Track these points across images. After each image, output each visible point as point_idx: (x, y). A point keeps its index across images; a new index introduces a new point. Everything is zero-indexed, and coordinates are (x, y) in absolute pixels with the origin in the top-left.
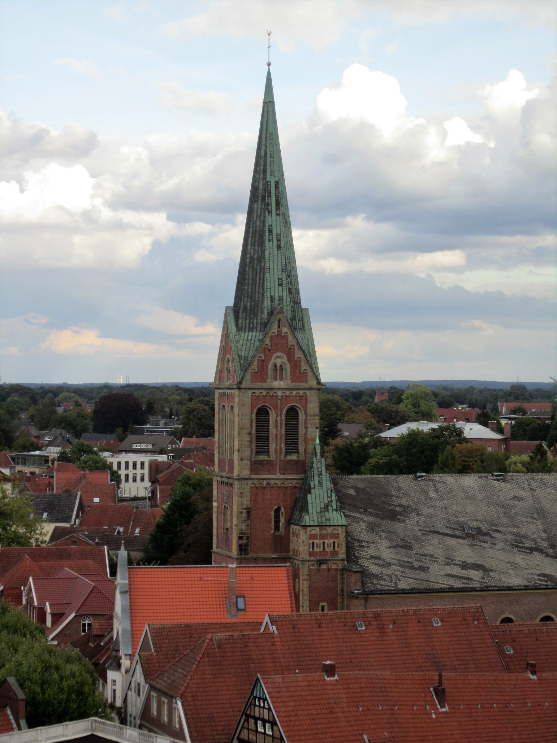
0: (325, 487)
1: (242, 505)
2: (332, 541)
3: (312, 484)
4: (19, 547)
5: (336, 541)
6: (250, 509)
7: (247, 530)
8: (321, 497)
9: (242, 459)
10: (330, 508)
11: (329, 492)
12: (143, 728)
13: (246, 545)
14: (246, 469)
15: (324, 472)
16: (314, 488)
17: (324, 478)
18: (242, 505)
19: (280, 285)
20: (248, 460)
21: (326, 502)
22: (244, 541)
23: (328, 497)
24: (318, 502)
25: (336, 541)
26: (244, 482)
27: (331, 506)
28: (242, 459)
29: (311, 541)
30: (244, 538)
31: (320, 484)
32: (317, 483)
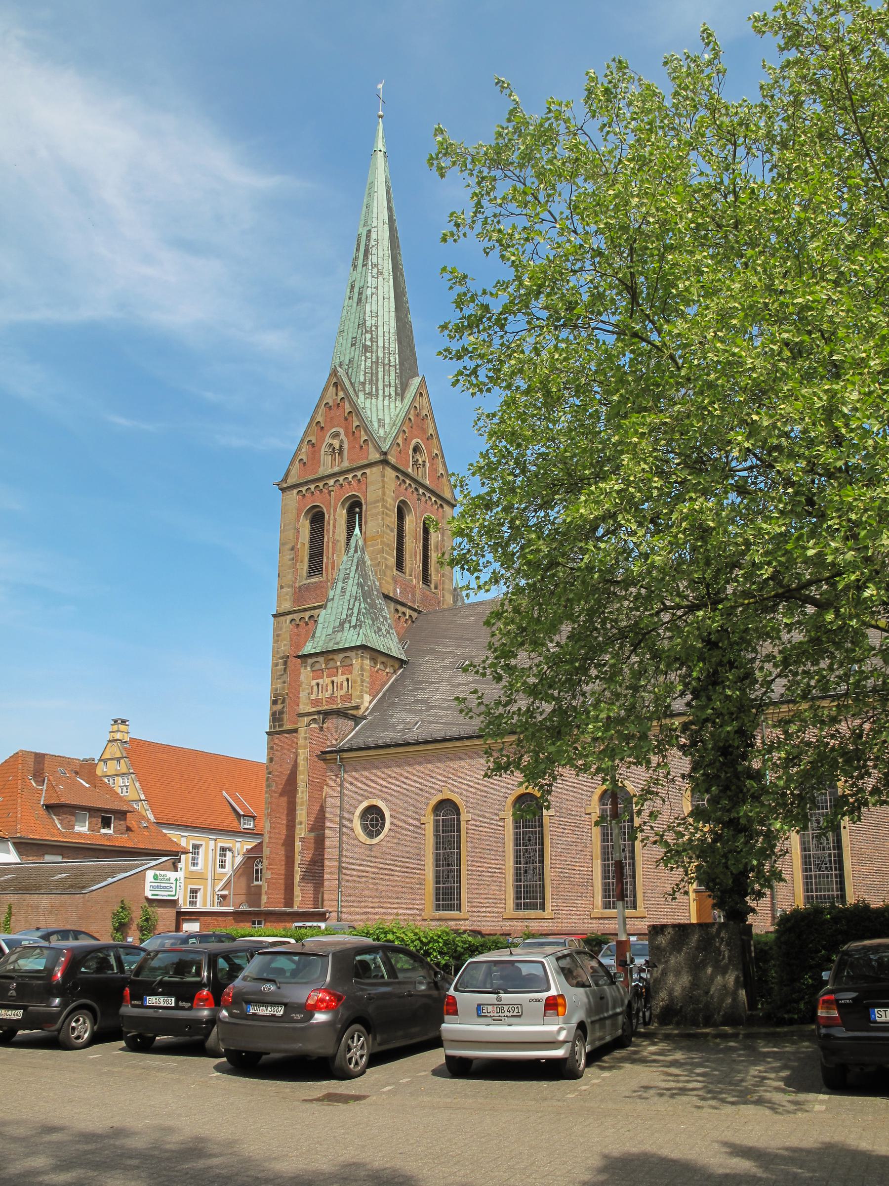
0: (348, 594)
1: (278, 652)
2: (345, 677)
3: (331, 594)
4: (805, 1114)
5: (349, 677)
6: (288, 657)
7: (283, 688)
8: (340, 610)
9: (282, 587)
10: (347, 625)
11: (352, 601)
12: (79, 937)
13: (281, 712)
14: (286, 600)
15: (352, 575)
16: (333, 599)
17: (350, 581)
18: (278, 652)
19: (353, 345)
20: (289, 587)
21: (344, 616)
22: (279, 707)
23: (349, 609)
24: (333, 618)
25: (349, 677)
26: (282, 618)
27: (350, 622)
28: (282, 587)
29: (314, 682)
30: (280, 702)
31: (343, 591)
32: (339, 590)
